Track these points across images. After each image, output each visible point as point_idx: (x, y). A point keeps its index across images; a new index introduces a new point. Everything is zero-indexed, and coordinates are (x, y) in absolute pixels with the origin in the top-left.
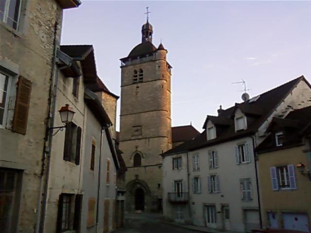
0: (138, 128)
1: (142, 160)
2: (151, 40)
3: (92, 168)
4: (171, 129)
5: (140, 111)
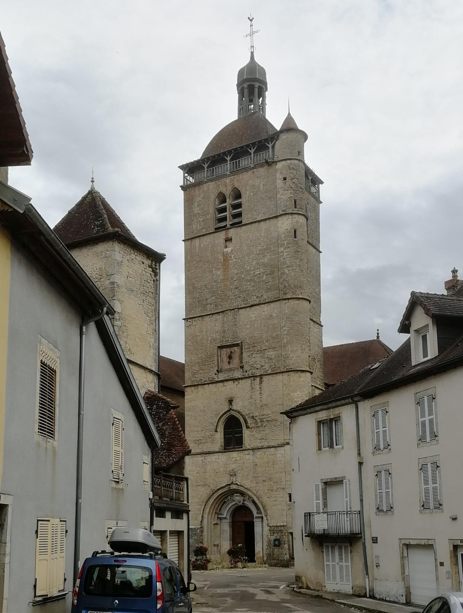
0: (231, 348)
1: (246, 433)
2: (263, 109)
3: (47, 427)
4: (321, 352)
5: (235, 305)
